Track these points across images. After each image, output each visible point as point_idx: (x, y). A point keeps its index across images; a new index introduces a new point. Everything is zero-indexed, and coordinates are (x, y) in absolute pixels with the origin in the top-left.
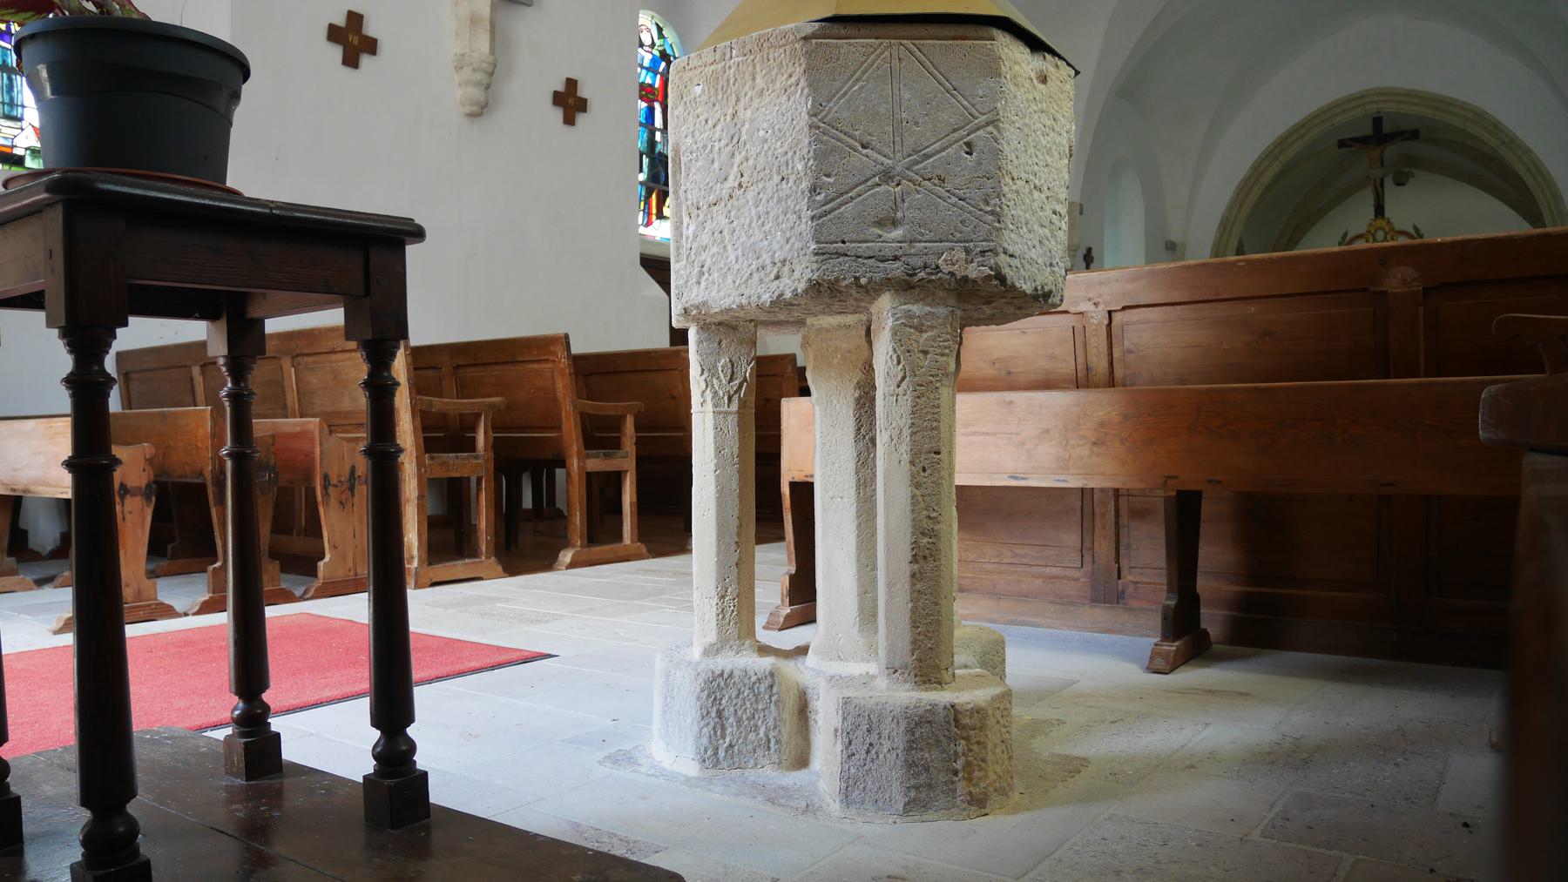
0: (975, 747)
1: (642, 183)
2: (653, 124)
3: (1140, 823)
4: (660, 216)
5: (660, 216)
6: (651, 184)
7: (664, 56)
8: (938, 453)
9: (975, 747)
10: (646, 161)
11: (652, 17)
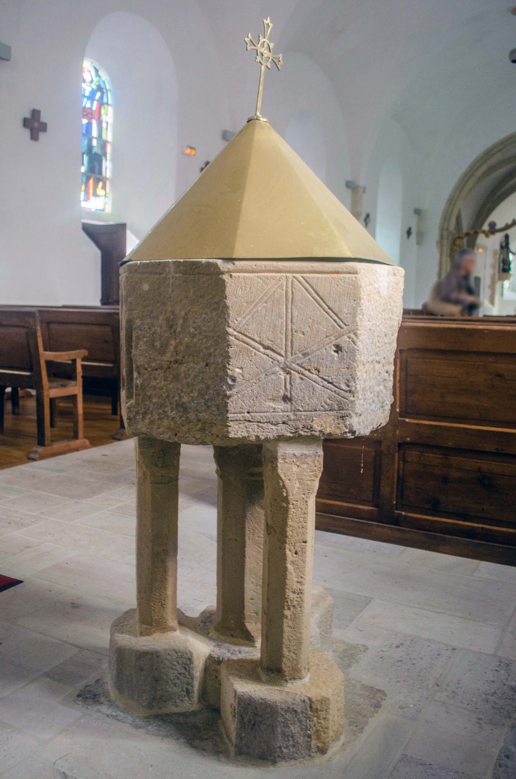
0: (322, 721)
1: (83, 174)
2: (91, 134)
3: (421, 764)
4: (95, 194)
5: (95, 194)
6: (89, 174)
7: (100, 89)
8: (305, 542)
9: (322, 721)
10: (86, 158)
11: (92, 63)
